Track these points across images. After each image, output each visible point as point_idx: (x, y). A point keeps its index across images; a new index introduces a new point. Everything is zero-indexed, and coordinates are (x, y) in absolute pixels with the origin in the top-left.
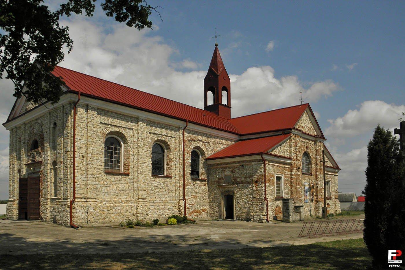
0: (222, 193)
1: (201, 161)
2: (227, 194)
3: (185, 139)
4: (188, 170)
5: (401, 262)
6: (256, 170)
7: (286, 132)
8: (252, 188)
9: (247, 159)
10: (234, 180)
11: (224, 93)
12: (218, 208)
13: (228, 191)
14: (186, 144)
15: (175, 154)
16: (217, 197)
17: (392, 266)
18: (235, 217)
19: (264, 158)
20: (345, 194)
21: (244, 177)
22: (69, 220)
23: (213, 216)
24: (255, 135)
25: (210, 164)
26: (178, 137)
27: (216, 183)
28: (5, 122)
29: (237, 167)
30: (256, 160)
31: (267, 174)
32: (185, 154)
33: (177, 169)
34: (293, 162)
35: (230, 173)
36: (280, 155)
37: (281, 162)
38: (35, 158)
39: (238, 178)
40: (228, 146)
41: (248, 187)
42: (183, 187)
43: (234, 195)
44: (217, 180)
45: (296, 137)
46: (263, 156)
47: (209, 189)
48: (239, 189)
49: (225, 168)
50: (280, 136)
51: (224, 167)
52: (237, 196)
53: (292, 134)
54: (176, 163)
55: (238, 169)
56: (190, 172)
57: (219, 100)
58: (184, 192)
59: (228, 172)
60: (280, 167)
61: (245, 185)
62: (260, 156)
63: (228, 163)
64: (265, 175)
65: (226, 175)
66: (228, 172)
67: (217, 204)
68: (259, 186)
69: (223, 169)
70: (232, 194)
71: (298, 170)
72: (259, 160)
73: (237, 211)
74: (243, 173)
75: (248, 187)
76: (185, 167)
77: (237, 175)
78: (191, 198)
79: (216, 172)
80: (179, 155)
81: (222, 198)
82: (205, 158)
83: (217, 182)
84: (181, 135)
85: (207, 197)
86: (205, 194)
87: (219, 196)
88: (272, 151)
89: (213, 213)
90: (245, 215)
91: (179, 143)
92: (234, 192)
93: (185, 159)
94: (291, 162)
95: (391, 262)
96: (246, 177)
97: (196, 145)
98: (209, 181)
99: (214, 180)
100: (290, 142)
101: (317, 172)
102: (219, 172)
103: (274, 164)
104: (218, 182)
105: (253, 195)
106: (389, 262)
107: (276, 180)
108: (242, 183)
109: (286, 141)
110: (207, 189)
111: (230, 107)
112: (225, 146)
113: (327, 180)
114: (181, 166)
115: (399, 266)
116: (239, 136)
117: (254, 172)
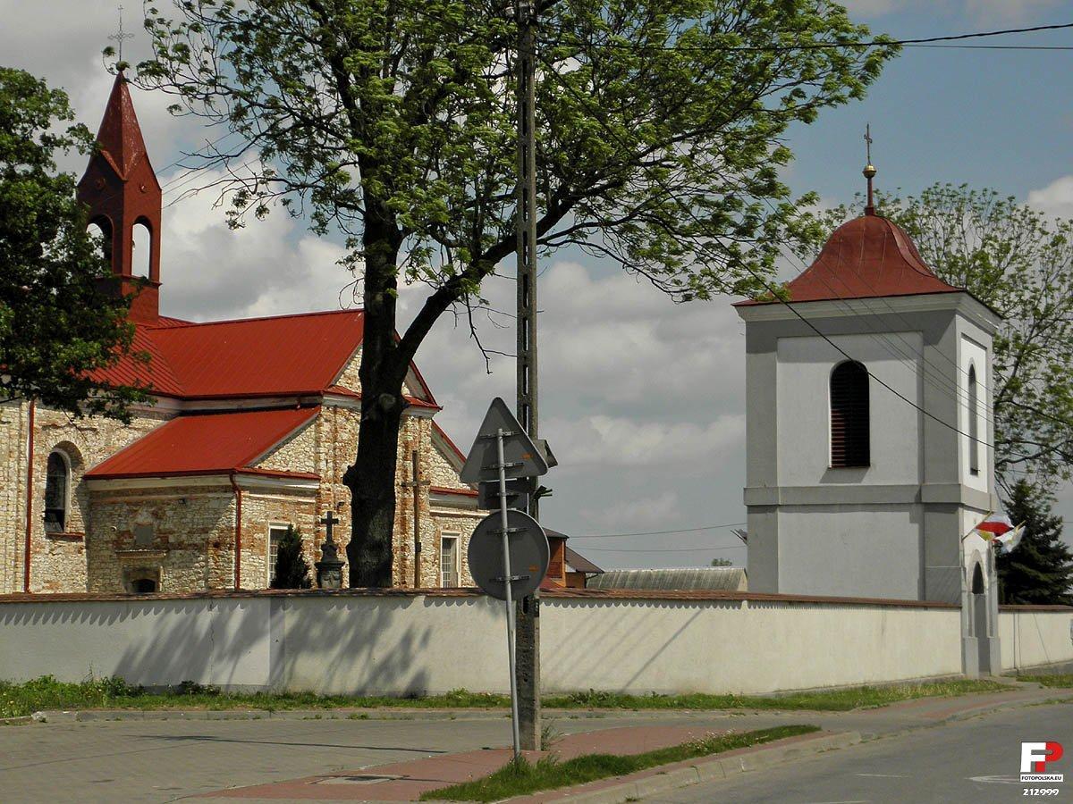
0: (127, 575)
1: (72, 481)
2: (141, 576)
3: (35, 425)
4: (39, 508)
6: (217, 513)
7: (307, 400)
8: (206, 561)
9: (196, 482)
11: (140, 233)
13: (144, 570)
14: (36, 437)
15: (9, 468)
16: (112, 585)
19: (237, 484)
20: (699, 578)
24: (223, 402)
25: (98, 492)
26: (17, 420)
29: (169, 504)
30: (219, 486)
31: (244, 525)
32: (34, 466)
33: (11, 509)
34: (323, 486)
35: (150, 520)
36: (285, 470)
37: (288, 490)
39: (172, 532)
40: (146, 434)
41: (195, 560)
42: (24, 559)
43: (159, 581)
44: (114, 537)
45: (335, 412)
46: (235, 475)
47: (89, 564)
49: (137, 504)
50: (289, 411)
51: (134, 502)
52: (166, 583)
53: (323, 409)
54: (11, 493)
55: (172, 509)
56: (43, 514)
57: (125, 267)
58: (27, 572)
59: (144, 517)
60: (283, 502)
61: (189, 552)
62: (228, 479)
63: (145, 492)
64: (238, 528)
65: (139, 525)
66: (144, 517)
68: (223, 557)
71: (338, 510)
72: (225, 489)
74: (184, 520)
75: (195, 560)
76: (33, 501)
77: (169, 526)
78: (43, 587)
79: (111, 514)
80: (19, 472)
82: (82, 473)
84: (25, 414)
85: (85, 586)
86: (78, 578)
88: (263, 460)
91: (21, 438)
93: (33, 480)
94: (318, 487)
96: (191, 533)
97: (61, 439)
98: (90, 539)
100: (318, 432)
101: (407, 511)
102: (120, 515)
103: (266, 496)
104: (118, 544)
105: (207, 581)
107: (271, 539)
109: (304, 429)
110: (86, 564)
111: (157, 285)
112: (138, 435)
113: (443, 534)
114: (23, 501)
116: (180, 402)
117: (211, 519)
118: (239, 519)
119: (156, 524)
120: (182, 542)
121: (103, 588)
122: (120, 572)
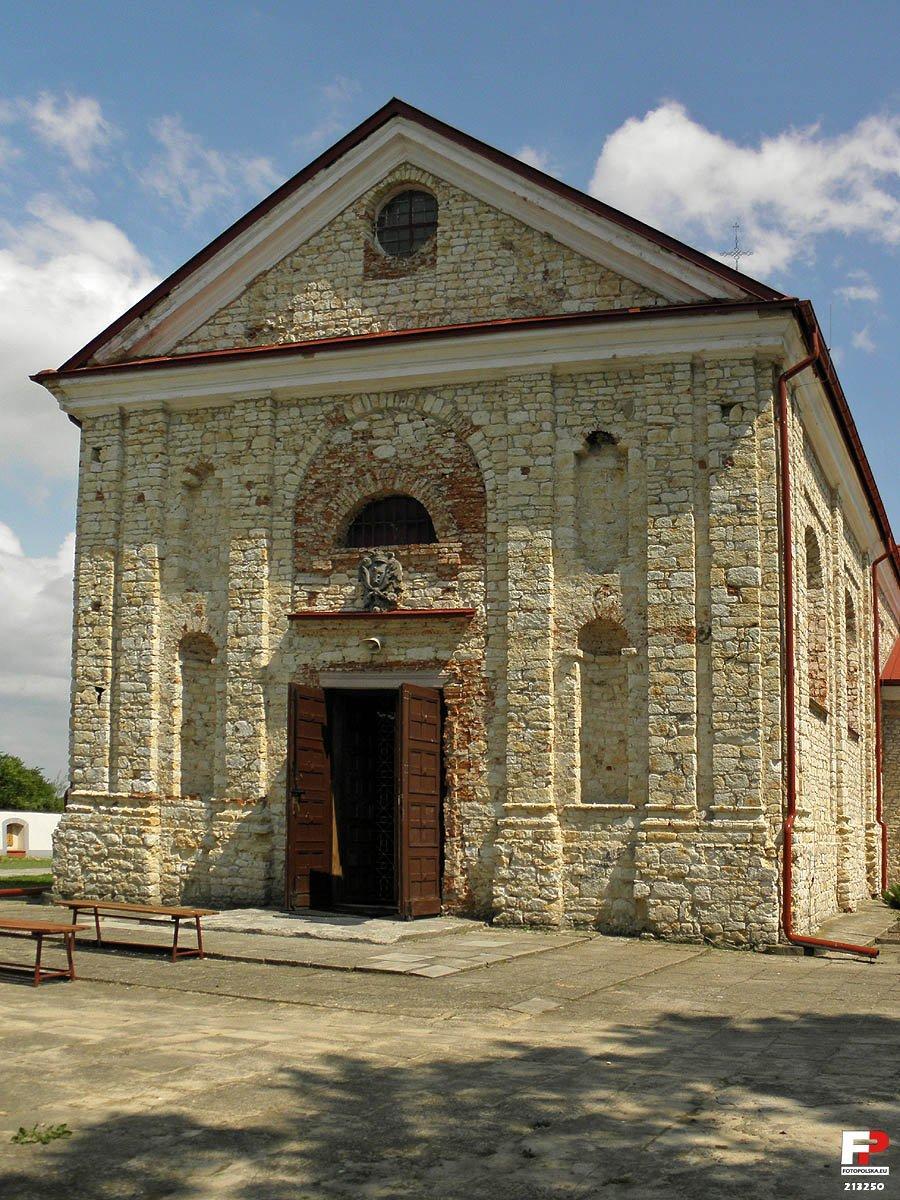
5: (887, 1174)
17: (854, 1184)
22: (775, 921)
28: (55, 367)
38: (398, 590)
95: (853, 1174)
106: (845, 1174)
115: (881, 1187)
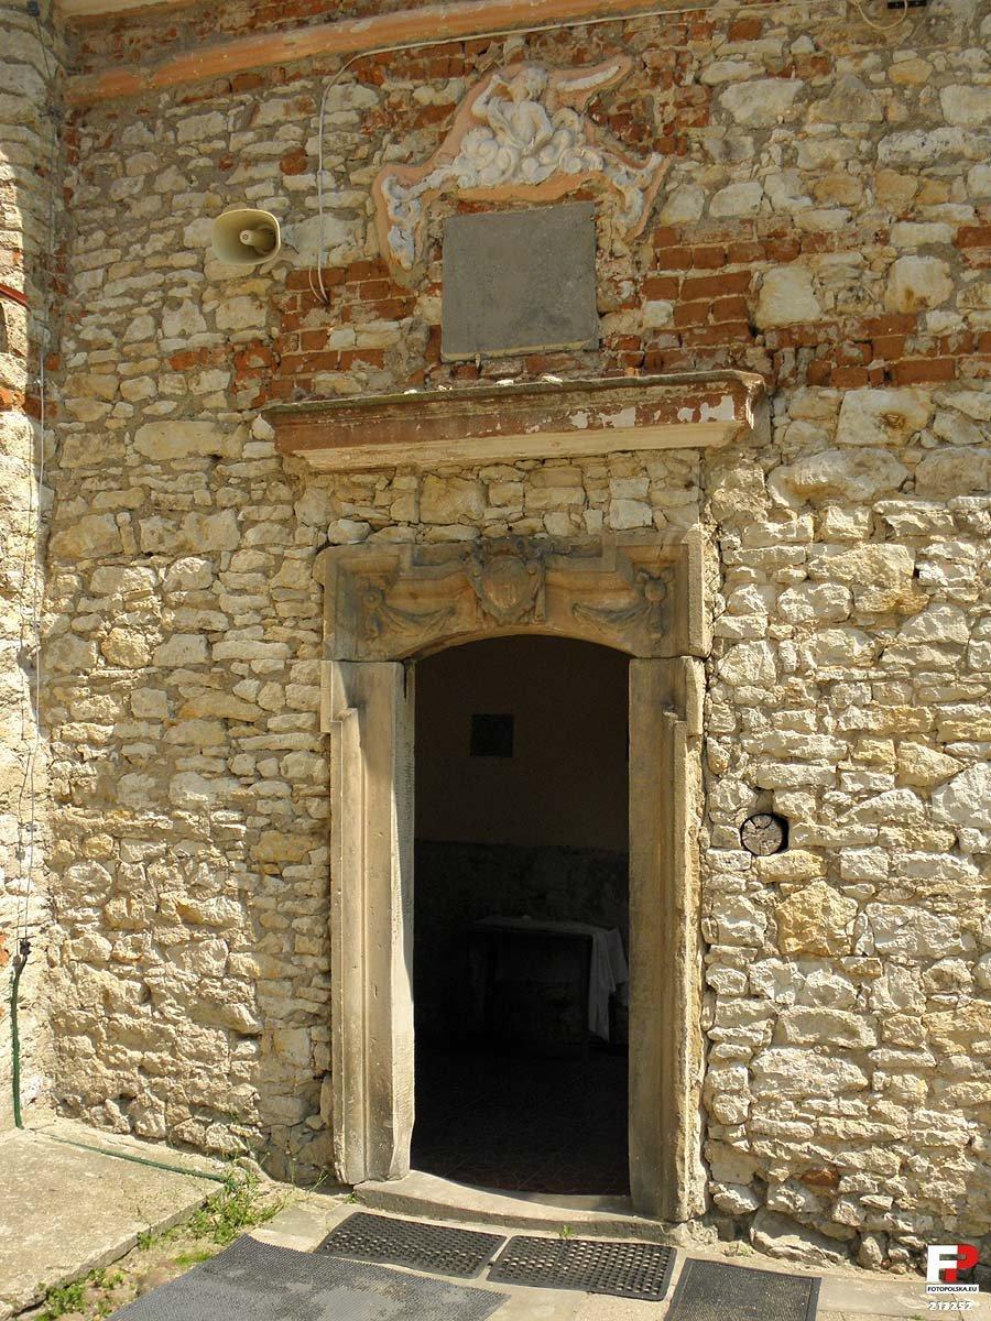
0: (358, 599)
2: (491, 609)
10: (657, 312)
12: (261, 929)
13: (520, 550)
16: (224, 675)
18: (693, 1185)
21: (941, 232)
23: (125, 1099)
27: (214, 380)
35: (578, 156)
39: (785, 246)
43: (684, 650)
44: (245, 318)
48: (812, 501)
65: (466, 206)
67: (219, 835)
69: (395, 86)
70: (614, 616)
73: (760, 1031)
79: (226, 163)
81: (357, 701)
83: (238, 357)
87: (268, 655)
89: (137, 1040)
90: (957, 1128)
92: (663, 587)
99: (173, 323)
102: (296, 161)
108: (887, 378)
118: (875, 446)
119: (630, 189)
120: (908, 322)
121: (151, 702)
122: (296, 573)
